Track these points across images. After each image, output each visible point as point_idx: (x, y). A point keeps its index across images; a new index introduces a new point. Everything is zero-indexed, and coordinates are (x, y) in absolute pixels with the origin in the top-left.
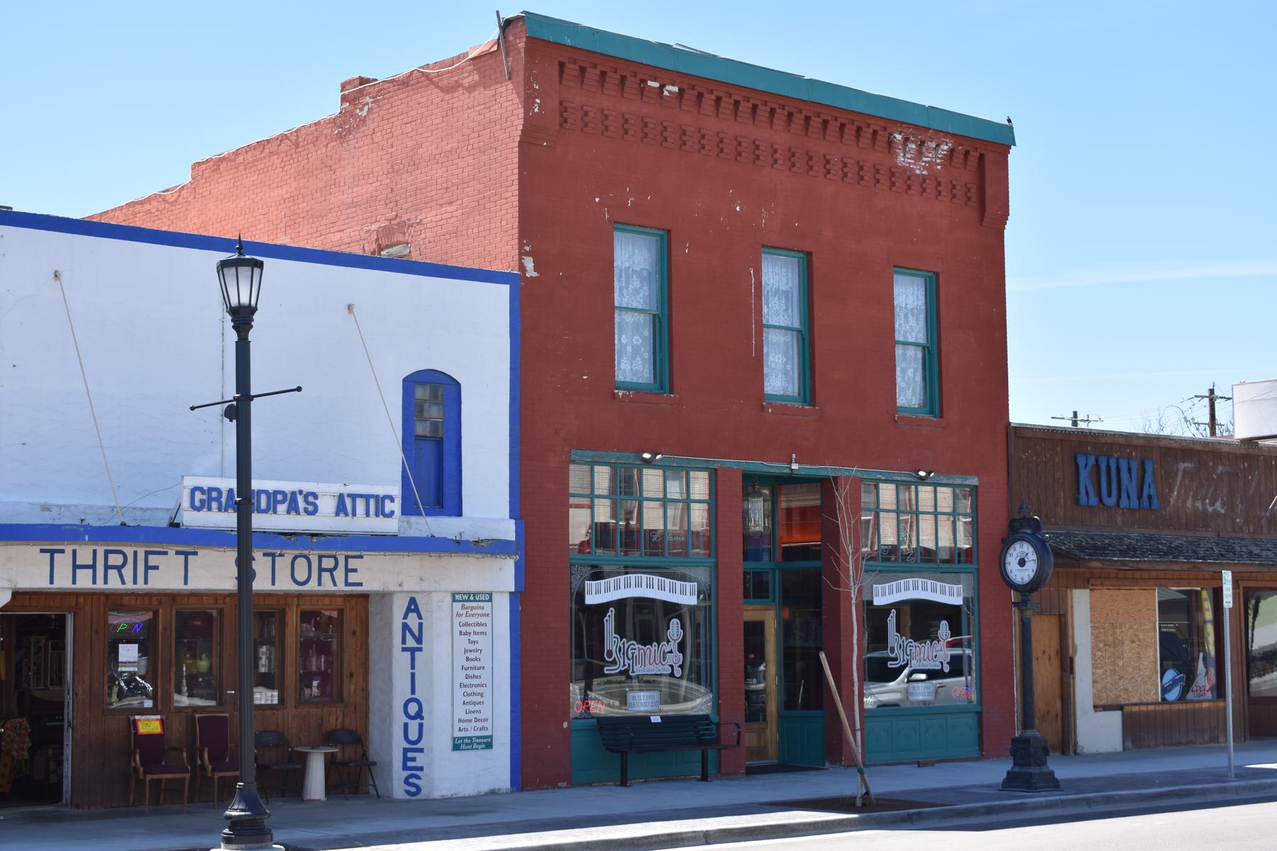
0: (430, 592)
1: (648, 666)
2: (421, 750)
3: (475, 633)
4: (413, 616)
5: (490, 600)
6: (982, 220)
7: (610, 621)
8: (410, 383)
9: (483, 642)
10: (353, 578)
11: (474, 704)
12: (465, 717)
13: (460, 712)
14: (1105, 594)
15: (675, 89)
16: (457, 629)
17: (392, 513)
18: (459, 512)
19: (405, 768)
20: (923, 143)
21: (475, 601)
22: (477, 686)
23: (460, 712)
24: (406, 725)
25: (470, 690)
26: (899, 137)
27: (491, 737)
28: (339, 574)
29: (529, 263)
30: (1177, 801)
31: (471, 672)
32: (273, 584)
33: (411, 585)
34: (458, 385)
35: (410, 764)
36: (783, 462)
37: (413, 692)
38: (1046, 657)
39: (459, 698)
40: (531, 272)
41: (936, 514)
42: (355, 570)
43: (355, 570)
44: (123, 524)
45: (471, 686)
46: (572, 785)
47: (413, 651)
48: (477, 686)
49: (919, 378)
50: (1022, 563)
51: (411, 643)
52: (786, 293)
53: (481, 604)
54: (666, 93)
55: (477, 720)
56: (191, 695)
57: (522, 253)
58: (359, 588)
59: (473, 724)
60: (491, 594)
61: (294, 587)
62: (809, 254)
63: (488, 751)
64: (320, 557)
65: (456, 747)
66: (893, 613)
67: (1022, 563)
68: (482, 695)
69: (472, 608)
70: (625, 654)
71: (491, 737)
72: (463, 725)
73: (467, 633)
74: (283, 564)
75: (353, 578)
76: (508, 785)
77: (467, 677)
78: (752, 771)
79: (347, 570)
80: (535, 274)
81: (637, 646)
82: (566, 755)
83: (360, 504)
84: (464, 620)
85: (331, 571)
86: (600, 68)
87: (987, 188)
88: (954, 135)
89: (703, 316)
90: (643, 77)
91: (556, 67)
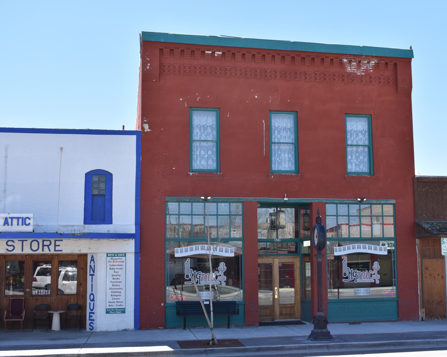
0: (97, 253)
1: (363, 279)
2: (93, 313)
3: (117, 269)
4: (92, 262)
5: (125, 256)
6: (397, 91)
8: (89, 176)
9: (121, 272)
10: (57, 248)
11: (117, 296)
12: (112, 301)
13: (110, 299)
16: (108, 267)
17: (29, 224)
18: (111, 223)
19: (90, 320)
20: (360, 62)
21: (118, 256)
23: (110, 299)
24: (90, 303)
25: (114, 291)
26: (345, 60)
27: (125, 309)
28: (52, 247)
29: (146, 127)
30: (392, 348)
31: (115, 284)
32: (22, 251)
33: (92, 251)
34: (111, 175)
35: (91, 318)
36: (281, 197)
37: (92, 291)
38: (440, 276)
39: (109, 292)
41: (205, 215)
42: (59, 246)
43: (59, 246)
44: (57, 232)
45: (115, 289)
46: (165, 327)
47: (92, 275)
49: (366, 160)
51: (92, 273)
52: (290, 129)
53: (120, 257)
54: (216, 55)
55: (117, 302)
56: (13, 290)
57: (143, 123)
58: (61, 252)
59: (116, 303)
60: (125, 254)
61: (31, 252)
62: (297, 112)
63: (123, 314)
64: (43, 241)
65: (107, 312)
68: (120, 292)
70: (353, 274)
71: (125, 309)
72: (111, 304)
73: (113, 269)
74: (27, 244)
75: (57, 248)
77: (113, 285)
78: (261, 324)
79: (55, 246)
81: (202, 273)
82: (151, 316)
83: (15, 221)
84: (112, 264)
87: (398, 77)
88: (376, 57)
91: (158, 51)
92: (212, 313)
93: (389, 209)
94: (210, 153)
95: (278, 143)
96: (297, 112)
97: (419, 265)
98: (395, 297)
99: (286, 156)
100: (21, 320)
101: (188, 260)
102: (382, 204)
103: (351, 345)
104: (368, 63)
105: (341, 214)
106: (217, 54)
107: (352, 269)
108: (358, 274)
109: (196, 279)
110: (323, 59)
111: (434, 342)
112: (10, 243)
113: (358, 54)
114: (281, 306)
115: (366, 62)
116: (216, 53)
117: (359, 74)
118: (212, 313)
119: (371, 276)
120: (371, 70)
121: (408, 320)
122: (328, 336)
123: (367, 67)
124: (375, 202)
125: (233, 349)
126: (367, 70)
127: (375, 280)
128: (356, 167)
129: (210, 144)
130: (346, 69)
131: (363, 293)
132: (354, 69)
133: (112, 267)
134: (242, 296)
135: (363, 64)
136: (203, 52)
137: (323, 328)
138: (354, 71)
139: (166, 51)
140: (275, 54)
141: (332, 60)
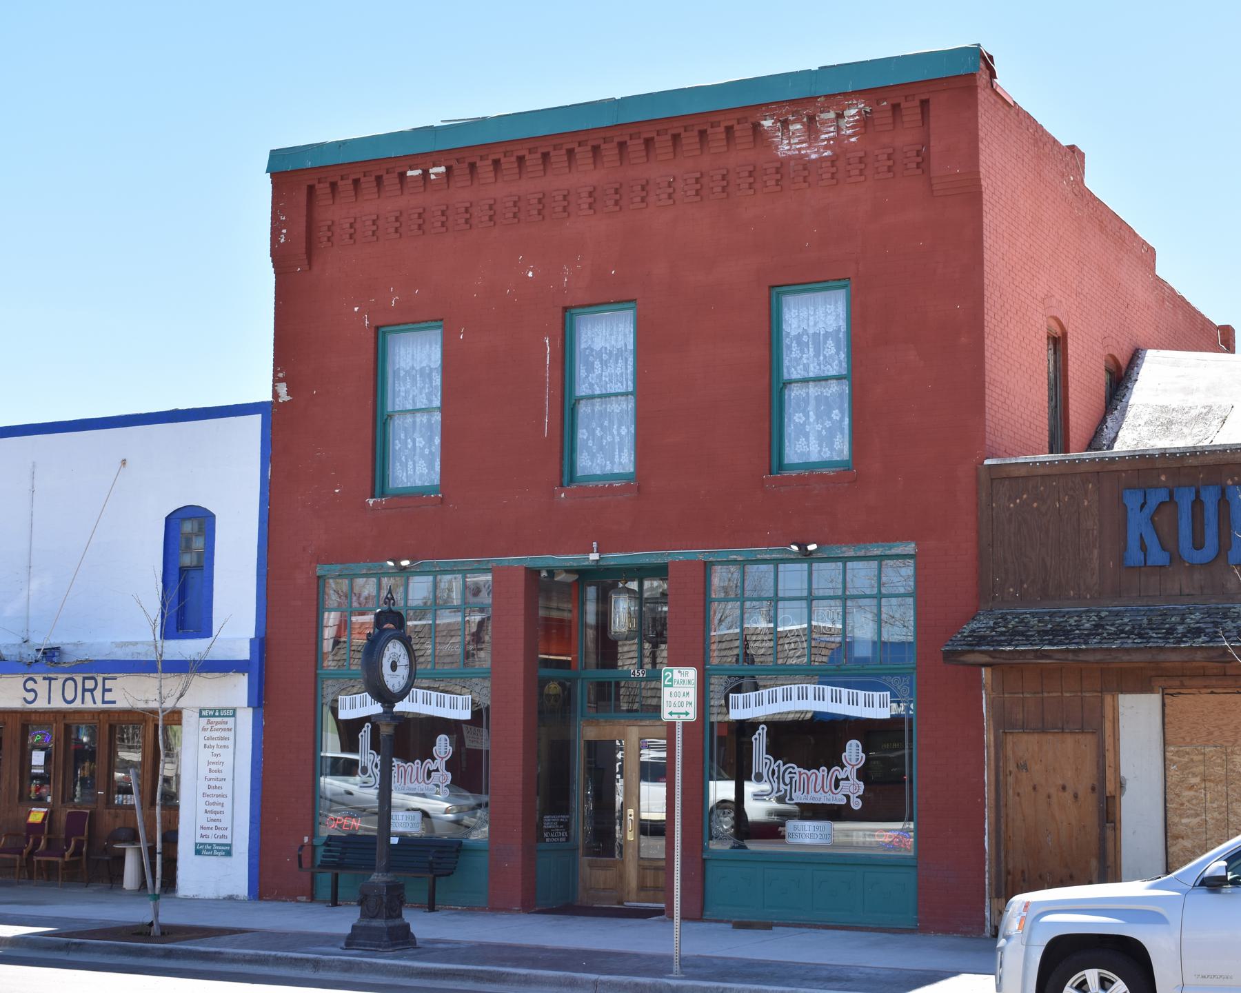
1: (812, 793)
3: (219, 747)
5: (234, 715)
7: (760, 741)
10: (108, 696)
11: (215, 813)
13: (202, 820)
14: (1199, 704)
15: (442, 169)
16: (202, 742)
20: (812, 119)
22: (218, 796)
25: (212, 800)
28: (98, 693)
29: (283, 388)
30: (308, 973)
31: (213, 783)
34: (213, 516)
38: (1068, 796)
40: (284, 397)
42: (110, 690)
43: (110, 690)
45: (213, 796)
48: (218, 796)
50: (394, 667)
54: (433, 177)
57: (276, 380)
59: (214, 832)
60: (234, 710)
61: (64, 705)
63: (227, 859)
65: (198, 852)
66: (367, 727)
67: (394, 667)
69: (217, 723)
71: (230, 845)
72: (204, 832)
73: (210, 747)
75: (108, 696)
76: (246, 892)
77: (210, 787)
79: (105, 690)
80: (288, 398)
81: (797, 770)
84: (208, 734)
85: (92, 691)
86: (670, 132)
89: (514, 405)
90: (401, 170)
92: (159, 857)
93: (901, 576)
94: (836, 415)
95: (601, 396)
96: (565, 309)
97: (989, 754)
98: (912, 854)
99: (420, 443)
100: (60, 860)
101: (760, 731)
102: (880, 558)
103: (370, 964)
104: (840, 116)
105: (787, 595)
106: (435, 174)
107: (780, 762)
108: (797, 777)
109: (782, 785)
110: (702, 133)
111: (588, 982)
112: (30, 685)
113: (802, 98)
114: (642, 862)
115: (832, 115)
116: (431, 171)
117: (813, 156)
118: (159, 857)
119: (837, 786)
120: (851, 136)
121: (946, 931)
122: (402, 939)
123: (839, 129)
124: (852, 554)
125: (120, 947)
126: (838, 138)
127: (848, 797)
128: (820, 446)
129: (833, 388)
130: (777, 148)
131: (812, 836)
132: (801, 142)
133: (208, 743)
134: (911, 841)
135: (824, 123)
136: (402, 175)
137: (375, 917)
138: (799, 150)
139: (323, 189)
140: (550, 149)
141: (729, 129)
